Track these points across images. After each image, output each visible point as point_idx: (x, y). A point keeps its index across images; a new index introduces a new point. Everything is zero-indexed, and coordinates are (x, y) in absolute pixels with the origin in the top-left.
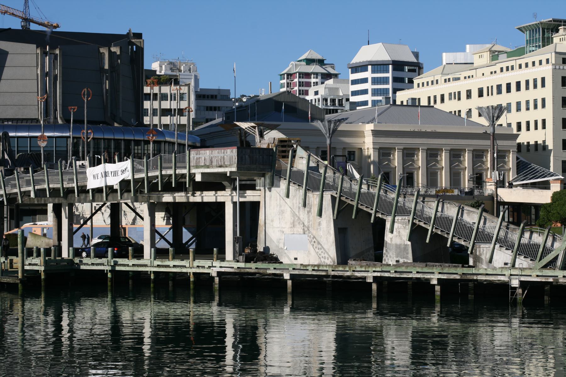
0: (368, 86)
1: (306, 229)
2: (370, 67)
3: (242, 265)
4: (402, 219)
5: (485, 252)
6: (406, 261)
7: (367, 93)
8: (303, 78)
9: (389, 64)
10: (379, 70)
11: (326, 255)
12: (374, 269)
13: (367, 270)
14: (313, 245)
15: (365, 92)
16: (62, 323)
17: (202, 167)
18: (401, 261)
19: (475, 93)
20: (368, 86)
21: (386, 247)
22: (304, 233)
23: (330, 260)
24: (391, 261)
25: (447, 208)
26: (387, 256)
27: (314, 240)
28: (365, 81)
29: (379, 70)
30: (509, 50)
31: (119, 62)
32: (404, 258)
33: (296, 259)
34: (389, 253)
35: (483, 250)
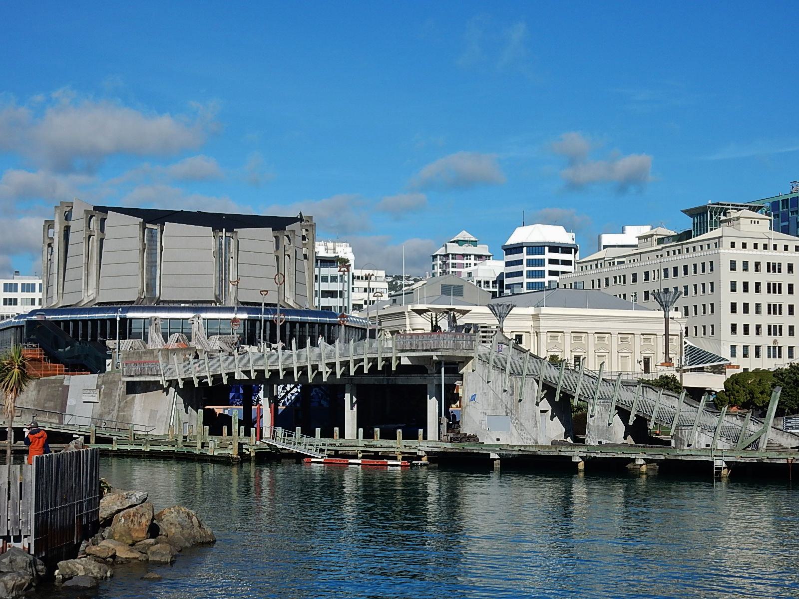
0: (548, 267)
1: (509, 411)
2: (525, 249)
3: (449, 445)
4: (604, 402)
5: (687, 434)
6: (608, 442)
7: (522, 275)
8: (455, 259)
9: (544, 246)
10: (534, 251)
11: (529, 437)
12: (580, 450)
13: (573, 450)
14: (516, 427)
15: (520, 274)
16: (129, 449)
17: (407, 351)
18: (604, 442)
19: (641, 277)
20: (548, 267)
21: (588, 429)
22: (507, 415)
23: (532, 441)
24: (594, 442)
25: (646, 391)
26: (589, 437)
27: (517, 421)
28: (520, 262)
29: (534, 251)
30: (673, 233)
31: (632, 234)
32: (606, 439)
33: (498, 440)
34: (591, 435)
35: (685, 432)
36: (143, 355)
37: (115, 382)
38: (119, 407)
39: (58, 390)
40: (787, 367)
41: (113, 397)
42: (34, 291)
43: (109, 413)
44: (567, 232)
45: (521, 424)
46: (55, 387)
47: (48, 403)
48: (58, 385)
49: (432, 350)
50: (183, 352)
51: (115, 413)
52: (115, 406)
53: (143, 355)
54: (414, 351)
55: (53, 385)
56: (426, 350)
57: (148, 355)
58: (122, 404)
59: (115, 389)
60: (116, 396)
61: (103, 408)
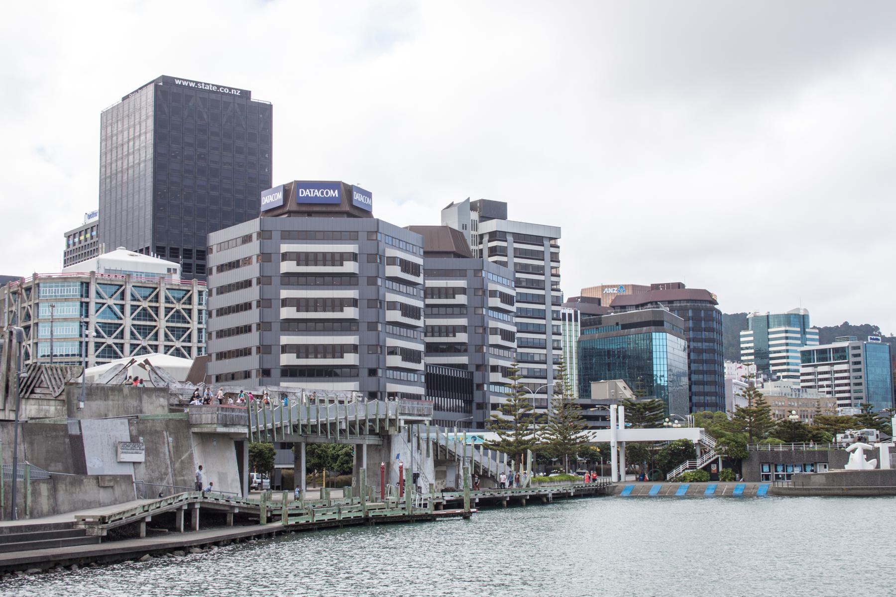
17: (405, 414)
36: (110, 393)
37: (156, 432)
38: (174, 470)
39: (64, 442)
40: (655, 373)
41: (162, 455)
42: (132, 300)
43: (162, 479)
44: (104, 115)
45: (426, 477)
46: (56, 437)
47: (53, 465)
48: (62, 433)
49: (424, 416)
50: (157, 394)
51: (170, 478)
52: (167, 467)
53: (110, 393)
54: (410, 415)
55: (54, 434)
56: (420, 415)
57: (116, 393)
58: (177, 465)
59: (161, 442)
60: (165, 454)
61: (150, 471)
